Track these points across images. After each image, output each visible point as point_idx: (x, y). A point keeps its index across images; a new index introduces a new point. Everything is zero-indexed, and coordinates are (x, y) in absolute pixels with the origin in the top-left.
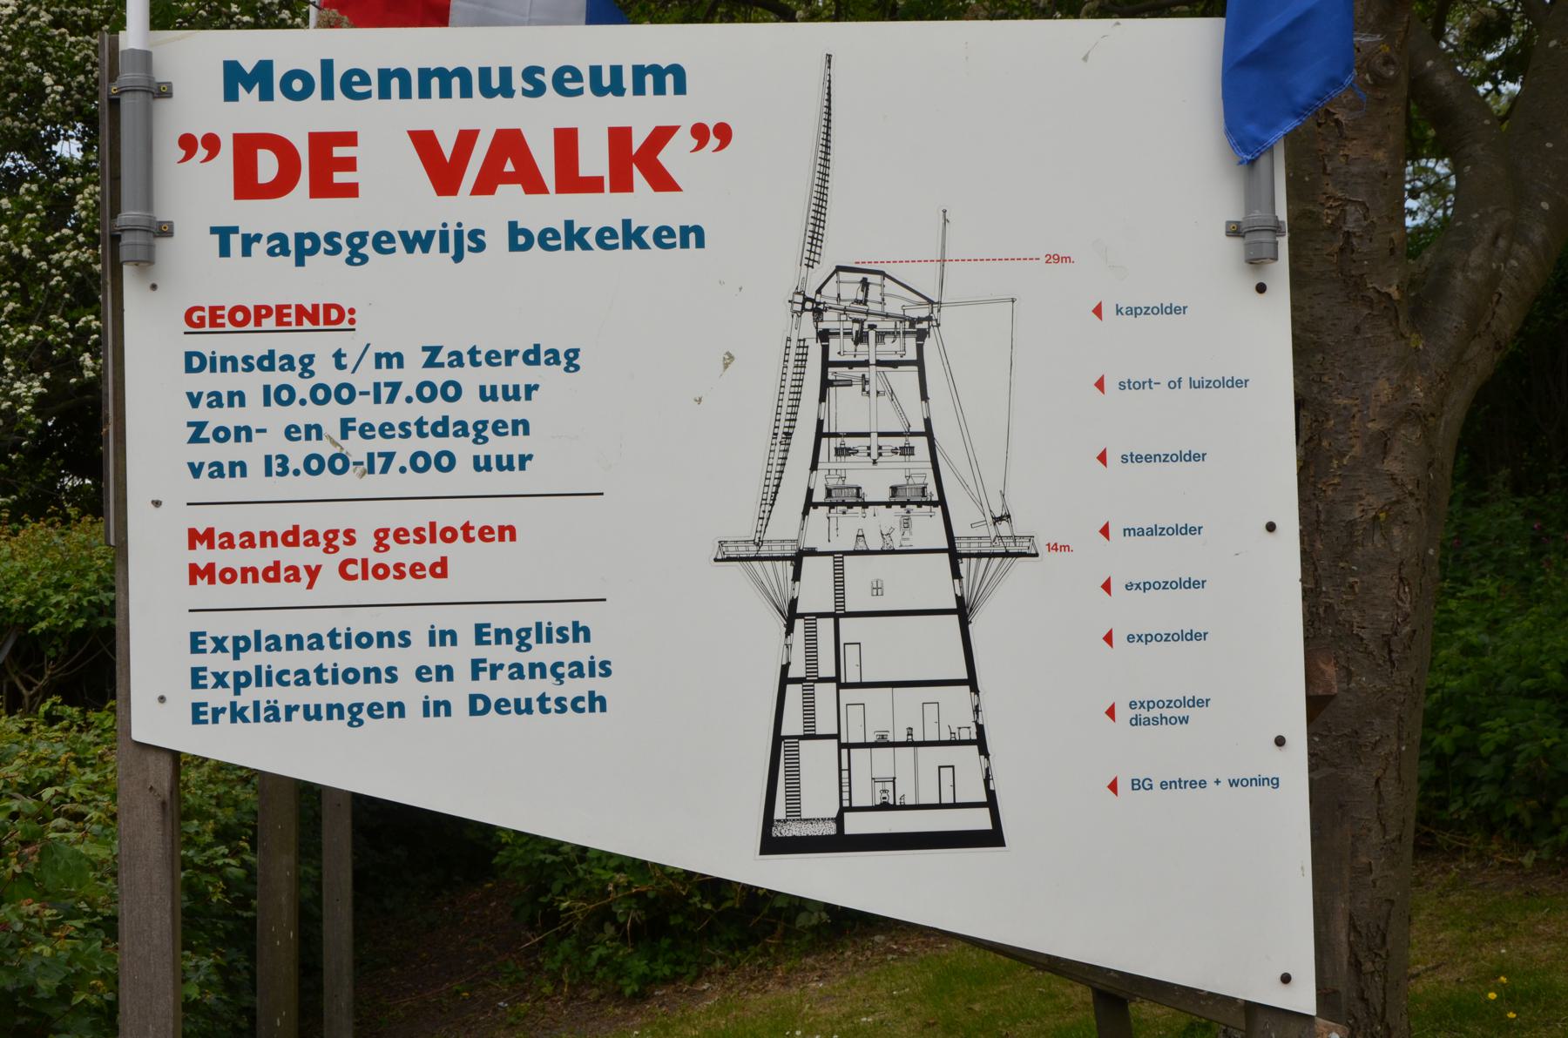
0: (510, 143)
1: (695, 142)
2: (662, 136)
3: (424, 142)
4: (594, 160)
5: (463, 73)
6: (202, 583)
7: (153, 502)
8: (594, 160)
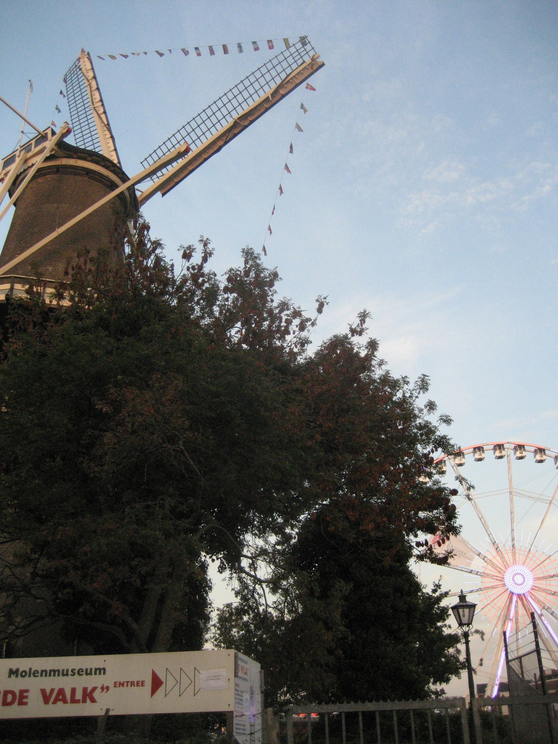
0: (61, 692)
1: (101, 691)
2: (94, 689)
4: (79, 695)
5: (58, 671)
6: (13, 677)
7: (253, 42)
8: (79, 695)
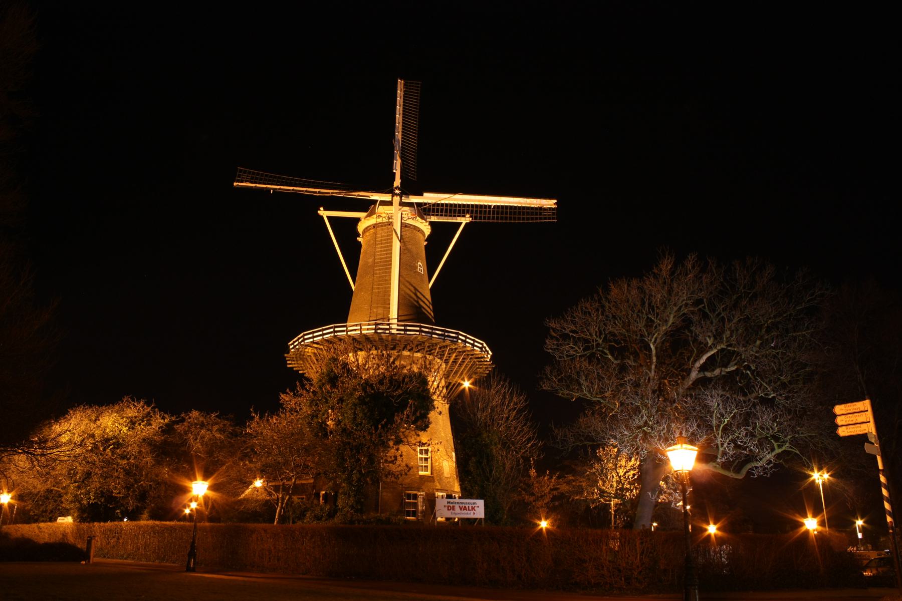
3: (460, 506)
